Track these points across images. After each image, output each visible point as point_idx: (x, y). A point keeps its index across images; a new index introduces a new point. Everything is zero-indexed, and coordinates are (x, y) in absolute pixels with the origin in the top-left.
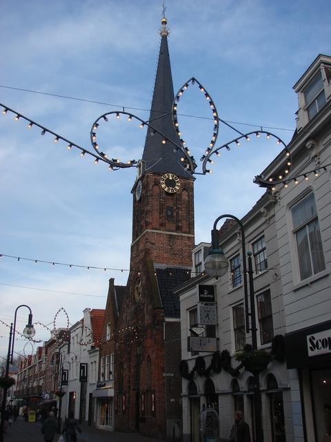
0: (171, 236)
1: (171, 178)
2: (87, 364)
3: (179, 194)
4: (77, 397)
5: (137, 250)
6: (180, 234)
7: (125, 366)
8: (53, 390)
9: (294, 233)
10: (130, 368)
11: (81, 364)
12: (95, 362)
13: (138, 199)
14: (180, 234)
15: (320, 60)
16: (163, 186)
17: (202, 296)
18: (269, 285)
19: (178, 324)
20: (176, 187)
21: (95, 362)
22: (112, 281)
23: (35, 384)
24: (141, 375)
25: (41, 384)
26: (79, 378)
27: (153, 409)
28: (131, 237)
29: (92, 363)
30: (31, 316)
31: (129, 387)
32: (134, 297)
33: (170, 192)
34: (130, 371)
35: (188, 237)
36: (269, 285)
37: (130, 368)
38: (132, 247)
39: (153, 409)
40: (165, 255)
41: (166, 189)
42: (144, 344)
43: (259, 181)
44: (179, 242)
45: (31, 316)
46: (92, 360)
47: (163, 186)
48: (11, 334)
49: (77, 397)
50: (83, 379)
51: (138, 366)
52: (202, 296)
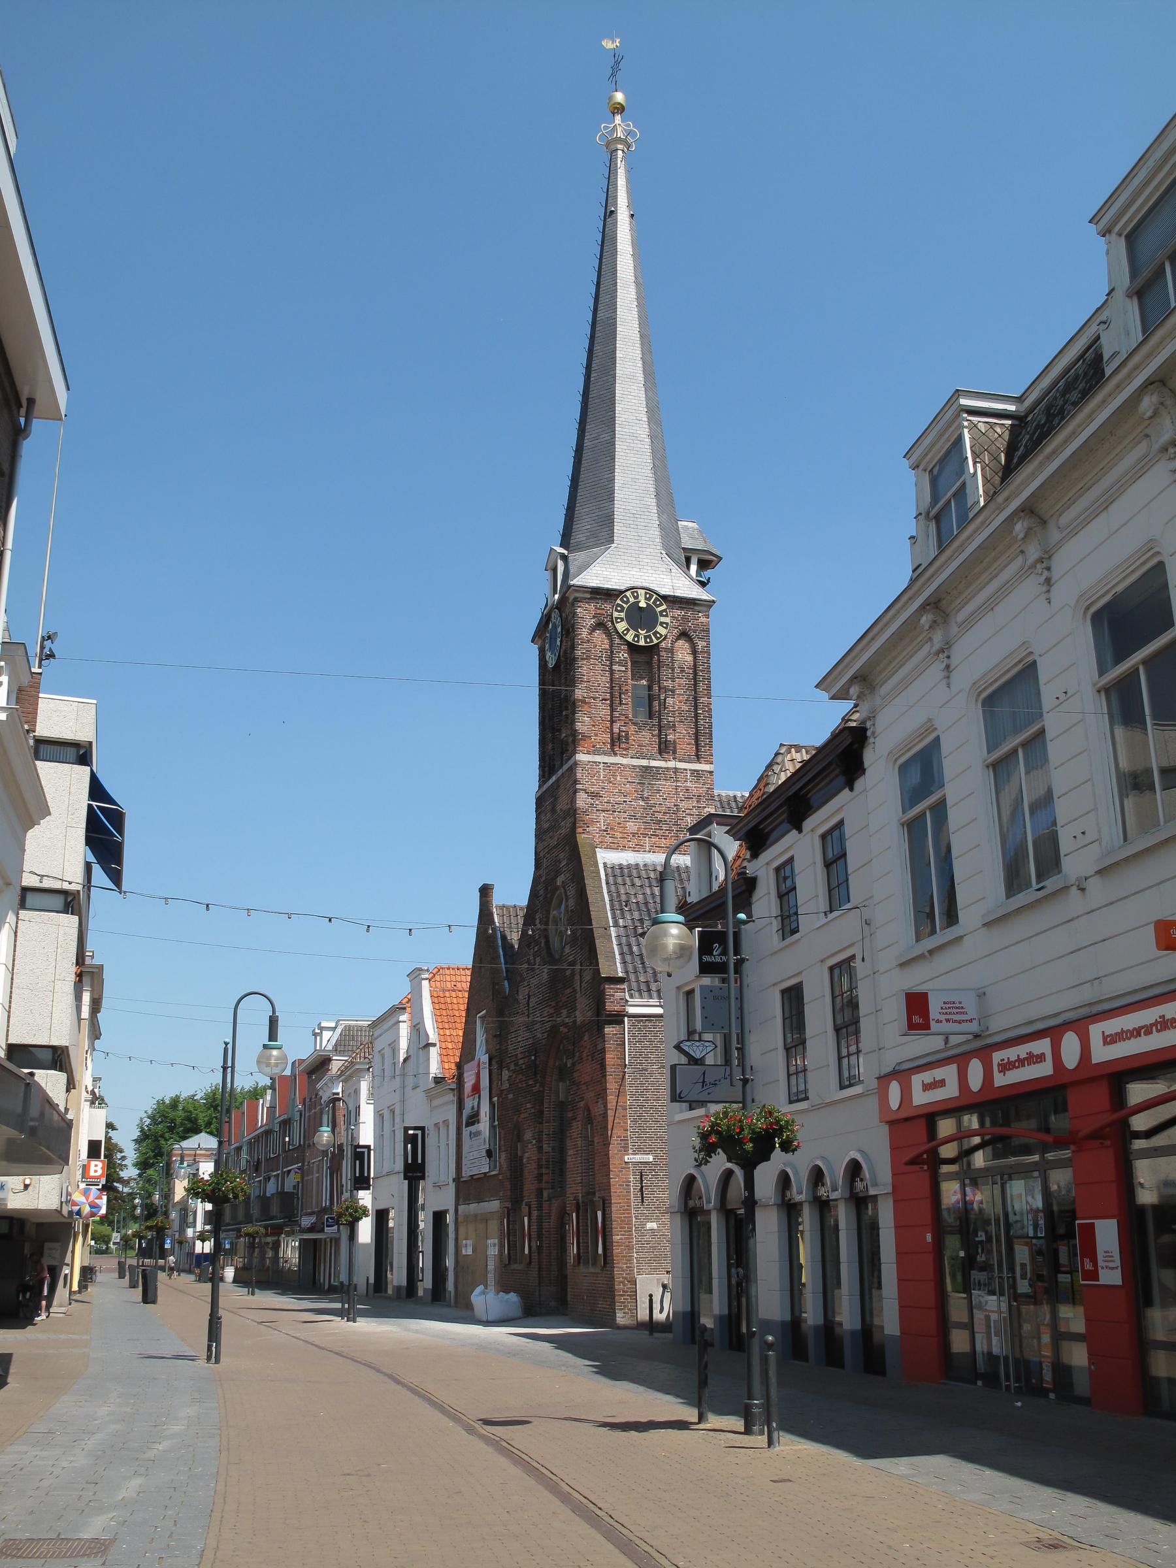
0: (647, 768)
1: (643, 604)
2: (422, 1129)
3: (666, 649)
4: (396, 1222)
5: (553, 810)
6: (671, 764)
7: (528, 1135)
8: (325, 1202)
9: (903, 825)
10: (540, 1141)
11: (406, 1129)
12: (446, 1122)
13: (551, 662)
14: (671, 764)
15: (955, 406)
16: (621, 626)
17: (706, 958)
18: (800, 973)
19: (1145, 662)
20: (659, 629)
21: (446, 1122)
22: (485, 891)
23: (271, 1188)
24: (569, 1159)
25: (288, 1188)
26: (400, 1166)
27: (526, 1252)
28: (536, 772)
29: (436, 1125)
30: (273, 1022)
31: (540, 1192)
32: (547, 942)
33: (642, 643)
34: (540, 1148)
35: (696, 774)
36: (800, 973)
37: (540, 1141)
38: (540, 801)
39: (526, 1252)
40: (632, 826)
41: (629, 637)
42: (576, 1075)
43: (833, 684)
44: (666, 786)
45: (273, 1022)
46: (439, 1119)
47: (621, 626)
48: (225, 1068)
49: (396, 1222)
50: (414, 1172)
51: (560, 1136)
52: (706, 958)
